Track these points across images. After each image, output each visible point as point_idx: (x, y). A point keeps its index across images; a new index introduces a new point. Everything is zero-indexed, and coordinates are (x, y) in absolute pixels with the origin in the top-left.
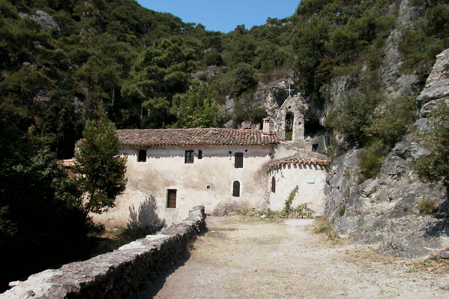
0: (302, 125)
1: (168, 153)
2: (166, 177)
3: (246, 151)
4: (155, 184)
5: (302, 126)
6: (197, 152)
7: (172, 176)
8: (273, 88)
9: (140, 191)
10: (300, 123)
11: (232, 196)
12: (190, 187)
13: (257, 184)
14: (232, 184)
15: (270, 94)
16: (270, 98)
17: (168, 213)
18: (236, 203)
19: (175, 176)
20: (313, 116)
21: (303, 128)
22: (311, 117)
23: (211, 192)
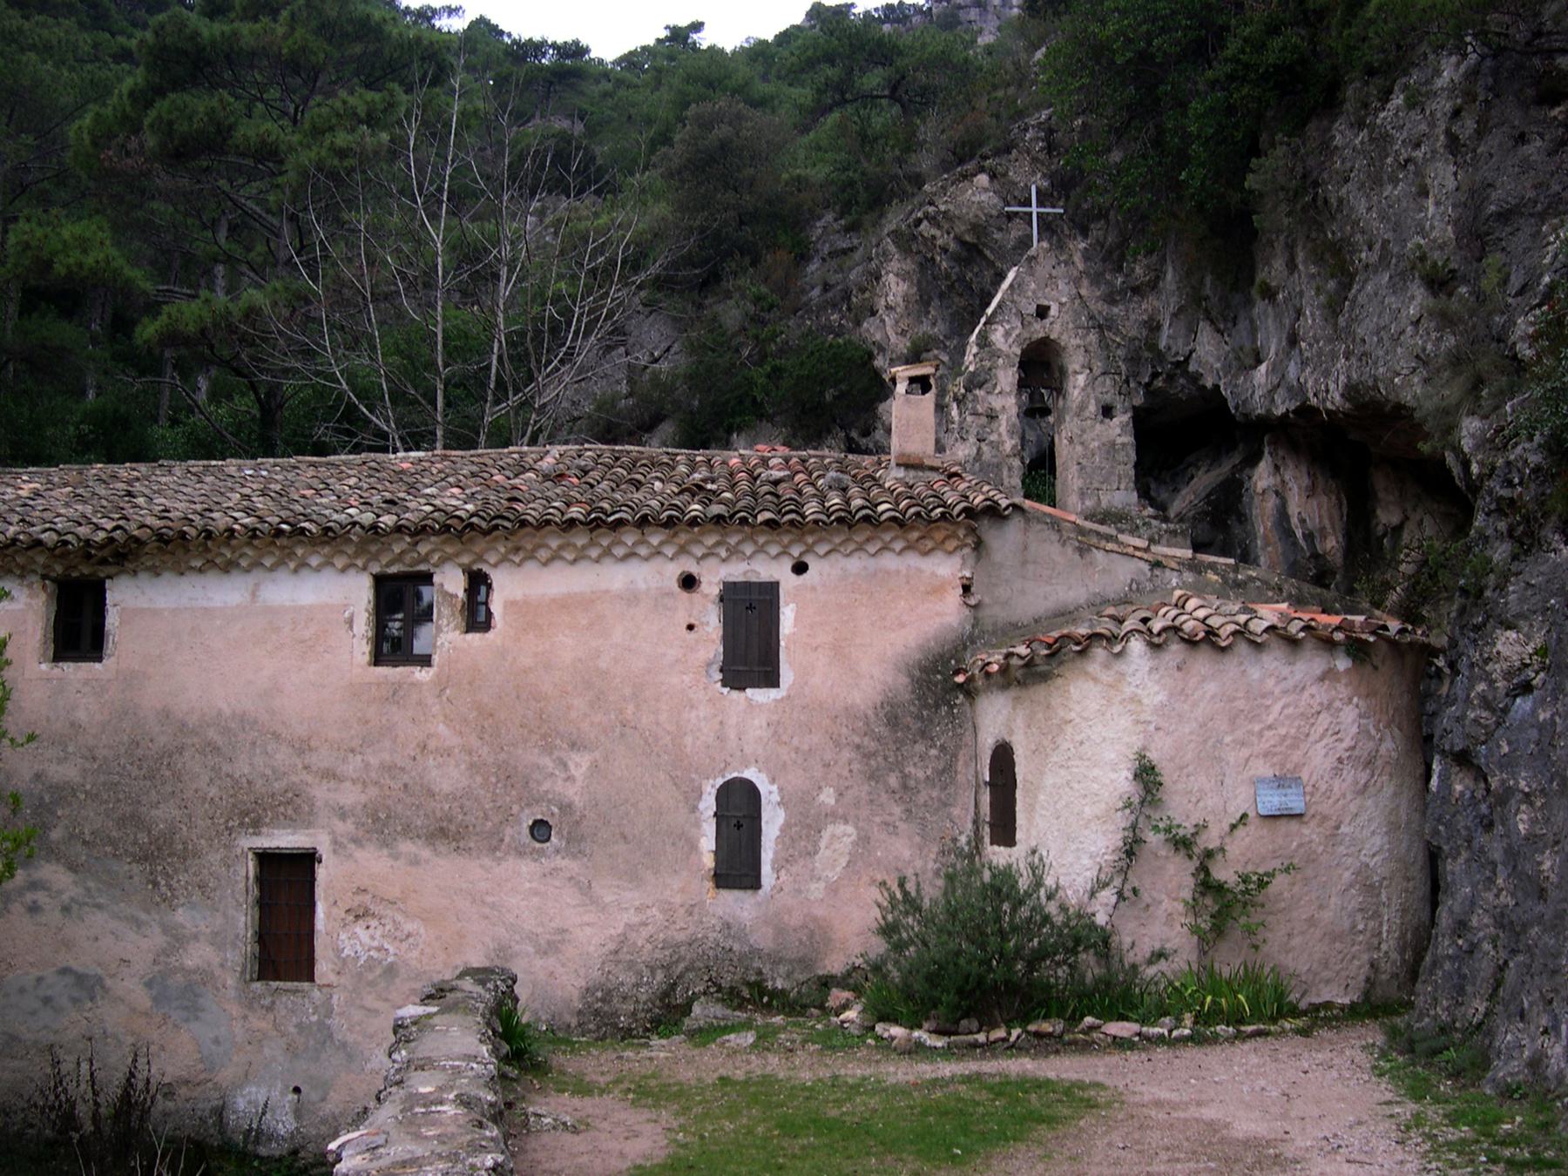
0: (1122, 418)
1: (254, 595)
2: (242, 768)
3: (800, 568)
4: (163, 814)
5: (1119, 430)
6: (451, 581)
7: (283, 756)
8: (919, 222)
9: (61, 869)
10: (1107, 411)
11: (710, 884)
12: (407, 831)
13: (884, 797)
14: (708, 804)
15: (894, 265)
16: (895, 288)
17: (259, 1023)
18: (741, 936)
19: (301, 752)
20: (1170, 378)
21: (1128, 439)
22: (1159, 383)
23: (559, 861)
